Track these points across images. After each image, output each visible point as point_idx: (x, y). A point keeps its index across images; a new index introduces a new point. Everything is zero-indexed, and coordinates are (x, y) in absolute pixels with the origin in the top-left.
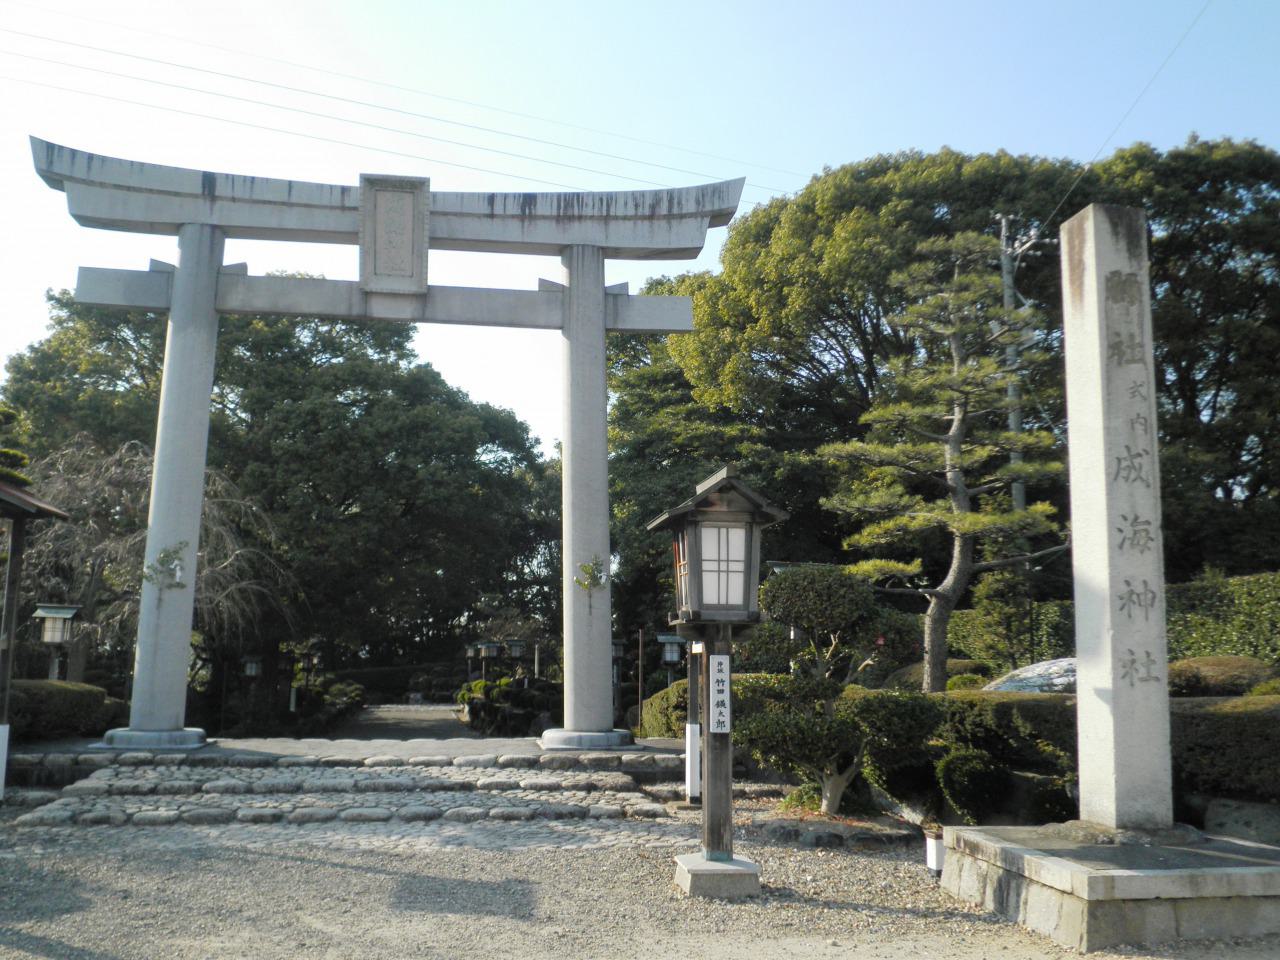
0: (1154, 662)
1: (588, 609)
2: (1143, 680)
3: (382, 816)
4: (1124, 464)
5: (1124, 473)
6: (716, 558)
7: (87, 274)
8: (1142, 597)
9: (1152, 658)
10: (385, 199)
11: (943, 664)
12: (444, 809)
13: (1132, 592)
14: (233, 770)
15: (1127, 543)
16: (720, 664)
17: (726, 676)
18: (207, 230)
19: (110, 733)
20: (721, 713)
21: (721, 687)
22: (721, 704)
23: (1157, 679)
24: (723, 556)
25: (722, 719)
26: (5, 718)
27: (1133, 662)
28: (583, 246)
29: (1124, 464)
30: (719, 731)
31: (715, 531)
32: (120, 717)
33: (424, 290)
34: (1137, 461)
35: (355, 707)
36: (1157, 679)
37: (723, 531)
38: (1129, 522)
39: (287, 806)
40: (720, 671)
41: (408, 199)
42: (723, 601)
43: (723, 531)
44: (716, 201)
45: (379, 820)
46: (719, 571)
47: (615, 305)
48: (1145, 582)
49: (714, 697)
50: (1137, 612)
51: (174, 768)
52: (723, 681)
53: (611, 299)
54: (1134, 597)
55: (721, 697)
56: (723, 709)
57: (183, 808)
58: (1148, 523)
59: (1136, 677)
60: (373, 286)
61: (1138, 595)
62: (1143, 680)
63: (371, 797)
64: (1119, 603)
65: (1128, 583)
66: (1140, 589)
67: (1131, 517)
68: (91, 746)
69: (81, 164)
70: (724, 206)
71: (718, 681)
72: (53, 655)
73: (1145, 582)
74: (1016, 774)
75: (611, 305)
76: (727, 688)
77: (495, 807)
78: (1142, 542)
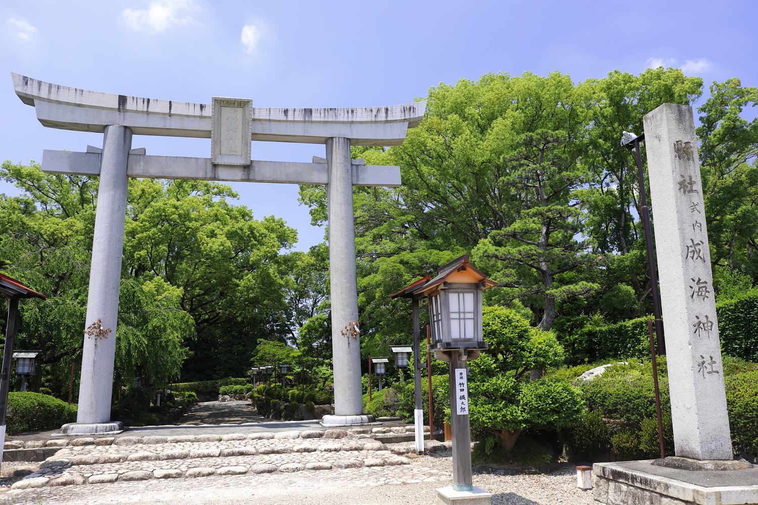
0: (715, 362)
1: (347, 345)
2: (709, 373)
3: (242, 471)
4: (691, 249)
5: (690, 255)
6: (457, 311)
7: (49, 154)
8: (706, 325)
9: (714, 360)
10: (226, 111)
11: (656, 368)
12: (278, 465)
13: (700, 323)
14: (145, 446)
15: (695, 294)
16: (461, 374)
17: (465, 381)
18: (123, 129)
19: (64, 426)
20: (463, 403)
21: (462, 388)
22: (463, 397)
23: (717, 372)
24: (462, 310)
25: (463, 406)
26: (4, 421)
27: (703, 363)
28: (339, 138)
29: (691, 249)
30: (462, 413)
31: (456, 295)
32: (72, 418)
33: (249, 163)
34: (697, 248)
35: (189, 404)
36: (717, 372)
37: (461, 295)
38: (696, 282)
39: (183, 468)
40: (461, 378)
41: (240, 110)
42: (463, 337)
43: (461, 295)
44: (412, 114)
45: (240, 473)
46: (459, 319)
47: (357, 171)
48: (707, 317)
49: (459, 394)
50: (703, 332)
51: (108, 447)
52: (463, 384)
53: (354, 167)
54: (701, 325)
55: (462, 394)
56: (463, 400)
57: (120, 472)
58: (706, 282)
59: (706, 371)
60: (219, 161)
61: (703, 324)
62: (709, 373)
63: (233, 459)
64: (694, 329)
65: (697, 317)
66: (704, 320)
67: (697, 280)
68: (52, 435)
69: (44, 89)
70: (417, 116)
71: (460, 384)
72: (23, 380)
73: (707, 317)
74: (637, 433)
75: (354, 170)
76: (465, 388)
77: (308, 462)
78: (703, 293)
